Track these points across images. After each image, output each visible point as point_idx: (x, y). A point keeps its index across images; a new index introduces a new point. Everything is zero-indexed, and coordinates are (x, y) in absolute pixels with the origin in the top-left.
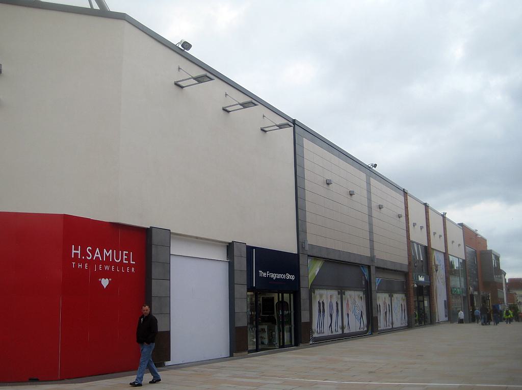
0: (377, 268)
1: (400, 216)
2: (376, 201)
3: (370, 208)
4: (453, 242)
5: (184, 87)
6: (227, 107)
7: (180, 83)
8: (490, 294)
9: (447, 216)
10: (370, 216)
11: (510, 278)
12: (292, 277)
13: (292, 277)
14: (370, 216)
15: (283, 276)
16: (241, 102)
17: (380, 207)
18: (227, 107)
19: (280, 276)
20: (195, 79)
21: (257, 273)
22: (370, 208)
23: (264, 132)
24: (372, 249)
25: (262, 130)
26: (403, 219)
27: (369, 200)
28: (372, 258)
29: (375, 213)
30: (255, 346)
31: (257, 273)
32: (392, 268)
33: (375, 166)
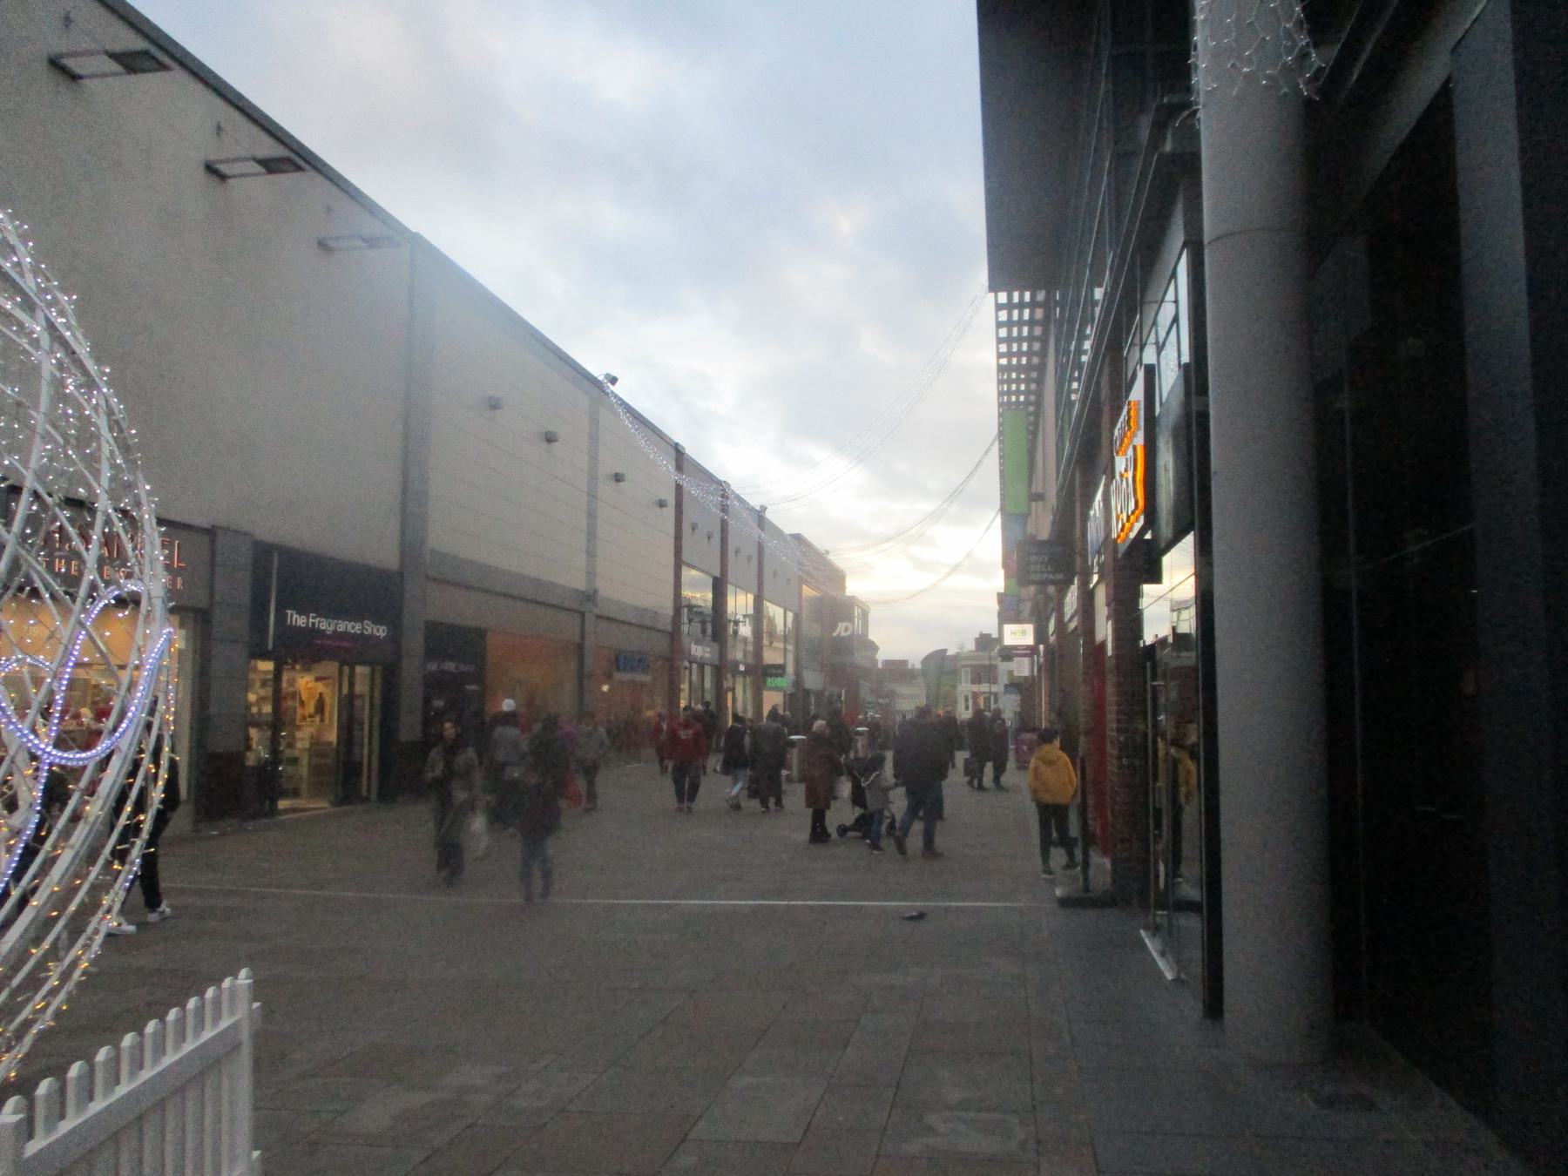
0: (599, 617)
1: (662, 504)
2: (608, 465)
3: (593, 478)
4: (775, 574)
5: (80, 77)
6: (75, 55)
7: (65, 61)
8: (843, 692)
9: (769, 515)
10: (592, 496)
11: (885, 659)
12: (381, 632)
13: (381, 632)
14: (592, 496)
15: (353, 627)
16: (118, 48)
17: (618, 478)
18: (221, 162)
19: (344, 626)
20: (260, 162)
21: (281, 617)
22: (593, 478)
23: (214, 181)
24: (591, 573)
25: (210, 169)
26: (670, 511)
27: (594, 457)
28: (590, 597)
29: (606, 490)
30: (710, 595)
31: (281, 617)
32: (64, 868)
33: (614, 380)
